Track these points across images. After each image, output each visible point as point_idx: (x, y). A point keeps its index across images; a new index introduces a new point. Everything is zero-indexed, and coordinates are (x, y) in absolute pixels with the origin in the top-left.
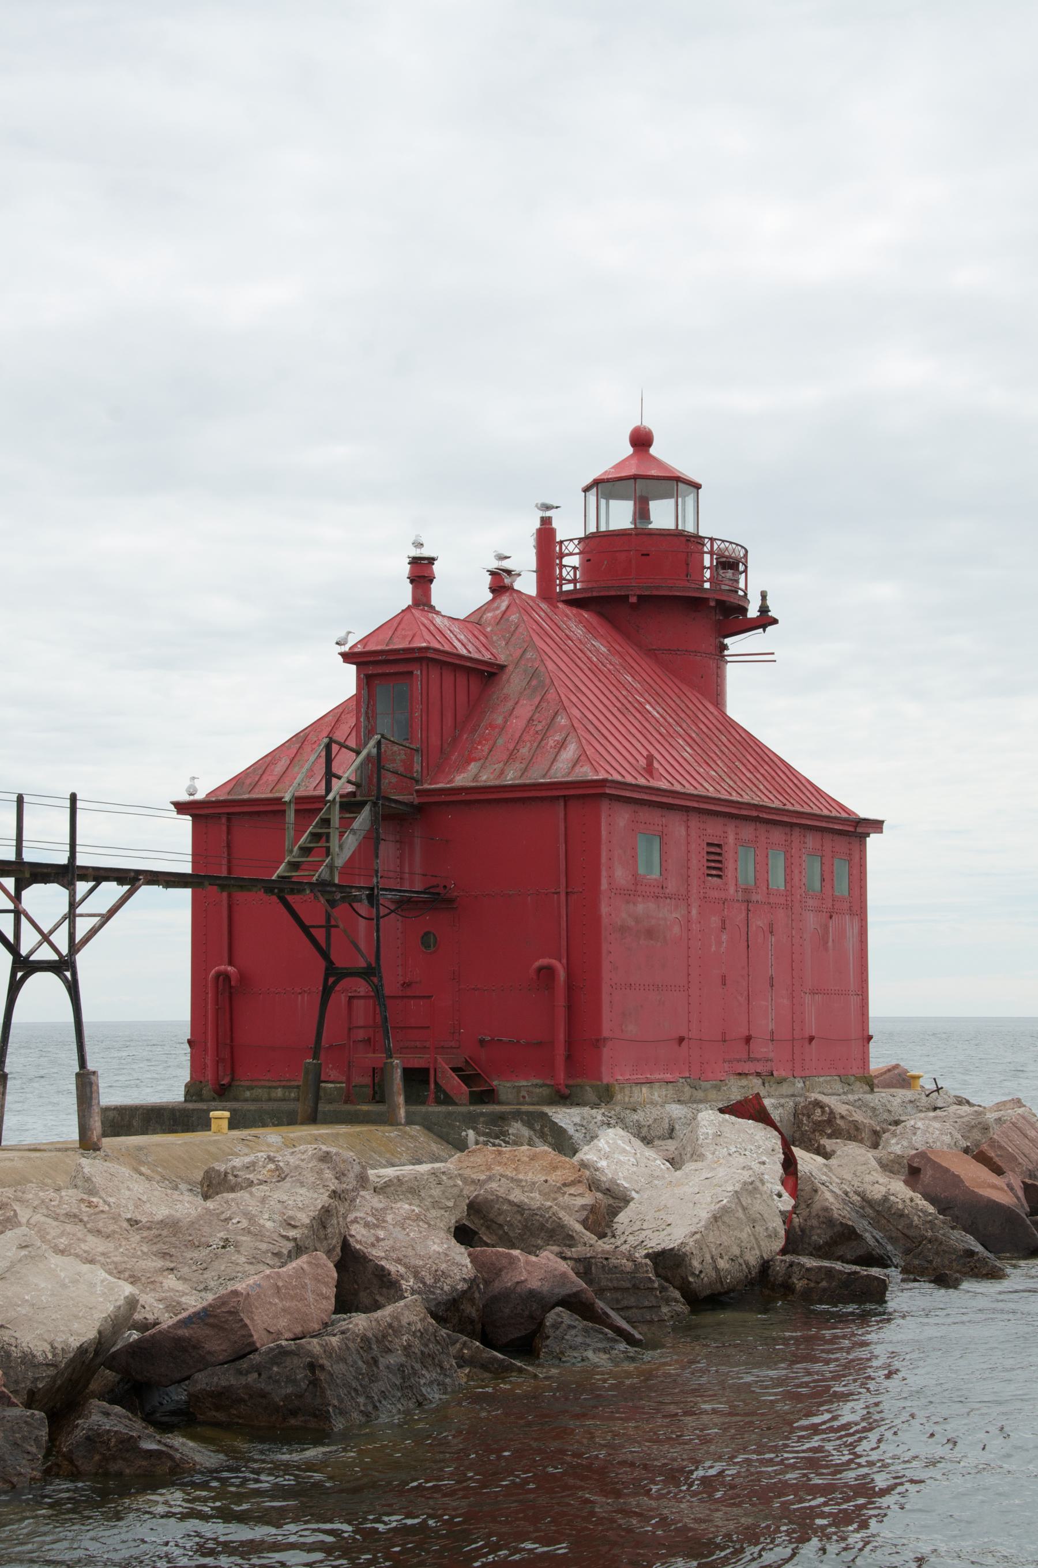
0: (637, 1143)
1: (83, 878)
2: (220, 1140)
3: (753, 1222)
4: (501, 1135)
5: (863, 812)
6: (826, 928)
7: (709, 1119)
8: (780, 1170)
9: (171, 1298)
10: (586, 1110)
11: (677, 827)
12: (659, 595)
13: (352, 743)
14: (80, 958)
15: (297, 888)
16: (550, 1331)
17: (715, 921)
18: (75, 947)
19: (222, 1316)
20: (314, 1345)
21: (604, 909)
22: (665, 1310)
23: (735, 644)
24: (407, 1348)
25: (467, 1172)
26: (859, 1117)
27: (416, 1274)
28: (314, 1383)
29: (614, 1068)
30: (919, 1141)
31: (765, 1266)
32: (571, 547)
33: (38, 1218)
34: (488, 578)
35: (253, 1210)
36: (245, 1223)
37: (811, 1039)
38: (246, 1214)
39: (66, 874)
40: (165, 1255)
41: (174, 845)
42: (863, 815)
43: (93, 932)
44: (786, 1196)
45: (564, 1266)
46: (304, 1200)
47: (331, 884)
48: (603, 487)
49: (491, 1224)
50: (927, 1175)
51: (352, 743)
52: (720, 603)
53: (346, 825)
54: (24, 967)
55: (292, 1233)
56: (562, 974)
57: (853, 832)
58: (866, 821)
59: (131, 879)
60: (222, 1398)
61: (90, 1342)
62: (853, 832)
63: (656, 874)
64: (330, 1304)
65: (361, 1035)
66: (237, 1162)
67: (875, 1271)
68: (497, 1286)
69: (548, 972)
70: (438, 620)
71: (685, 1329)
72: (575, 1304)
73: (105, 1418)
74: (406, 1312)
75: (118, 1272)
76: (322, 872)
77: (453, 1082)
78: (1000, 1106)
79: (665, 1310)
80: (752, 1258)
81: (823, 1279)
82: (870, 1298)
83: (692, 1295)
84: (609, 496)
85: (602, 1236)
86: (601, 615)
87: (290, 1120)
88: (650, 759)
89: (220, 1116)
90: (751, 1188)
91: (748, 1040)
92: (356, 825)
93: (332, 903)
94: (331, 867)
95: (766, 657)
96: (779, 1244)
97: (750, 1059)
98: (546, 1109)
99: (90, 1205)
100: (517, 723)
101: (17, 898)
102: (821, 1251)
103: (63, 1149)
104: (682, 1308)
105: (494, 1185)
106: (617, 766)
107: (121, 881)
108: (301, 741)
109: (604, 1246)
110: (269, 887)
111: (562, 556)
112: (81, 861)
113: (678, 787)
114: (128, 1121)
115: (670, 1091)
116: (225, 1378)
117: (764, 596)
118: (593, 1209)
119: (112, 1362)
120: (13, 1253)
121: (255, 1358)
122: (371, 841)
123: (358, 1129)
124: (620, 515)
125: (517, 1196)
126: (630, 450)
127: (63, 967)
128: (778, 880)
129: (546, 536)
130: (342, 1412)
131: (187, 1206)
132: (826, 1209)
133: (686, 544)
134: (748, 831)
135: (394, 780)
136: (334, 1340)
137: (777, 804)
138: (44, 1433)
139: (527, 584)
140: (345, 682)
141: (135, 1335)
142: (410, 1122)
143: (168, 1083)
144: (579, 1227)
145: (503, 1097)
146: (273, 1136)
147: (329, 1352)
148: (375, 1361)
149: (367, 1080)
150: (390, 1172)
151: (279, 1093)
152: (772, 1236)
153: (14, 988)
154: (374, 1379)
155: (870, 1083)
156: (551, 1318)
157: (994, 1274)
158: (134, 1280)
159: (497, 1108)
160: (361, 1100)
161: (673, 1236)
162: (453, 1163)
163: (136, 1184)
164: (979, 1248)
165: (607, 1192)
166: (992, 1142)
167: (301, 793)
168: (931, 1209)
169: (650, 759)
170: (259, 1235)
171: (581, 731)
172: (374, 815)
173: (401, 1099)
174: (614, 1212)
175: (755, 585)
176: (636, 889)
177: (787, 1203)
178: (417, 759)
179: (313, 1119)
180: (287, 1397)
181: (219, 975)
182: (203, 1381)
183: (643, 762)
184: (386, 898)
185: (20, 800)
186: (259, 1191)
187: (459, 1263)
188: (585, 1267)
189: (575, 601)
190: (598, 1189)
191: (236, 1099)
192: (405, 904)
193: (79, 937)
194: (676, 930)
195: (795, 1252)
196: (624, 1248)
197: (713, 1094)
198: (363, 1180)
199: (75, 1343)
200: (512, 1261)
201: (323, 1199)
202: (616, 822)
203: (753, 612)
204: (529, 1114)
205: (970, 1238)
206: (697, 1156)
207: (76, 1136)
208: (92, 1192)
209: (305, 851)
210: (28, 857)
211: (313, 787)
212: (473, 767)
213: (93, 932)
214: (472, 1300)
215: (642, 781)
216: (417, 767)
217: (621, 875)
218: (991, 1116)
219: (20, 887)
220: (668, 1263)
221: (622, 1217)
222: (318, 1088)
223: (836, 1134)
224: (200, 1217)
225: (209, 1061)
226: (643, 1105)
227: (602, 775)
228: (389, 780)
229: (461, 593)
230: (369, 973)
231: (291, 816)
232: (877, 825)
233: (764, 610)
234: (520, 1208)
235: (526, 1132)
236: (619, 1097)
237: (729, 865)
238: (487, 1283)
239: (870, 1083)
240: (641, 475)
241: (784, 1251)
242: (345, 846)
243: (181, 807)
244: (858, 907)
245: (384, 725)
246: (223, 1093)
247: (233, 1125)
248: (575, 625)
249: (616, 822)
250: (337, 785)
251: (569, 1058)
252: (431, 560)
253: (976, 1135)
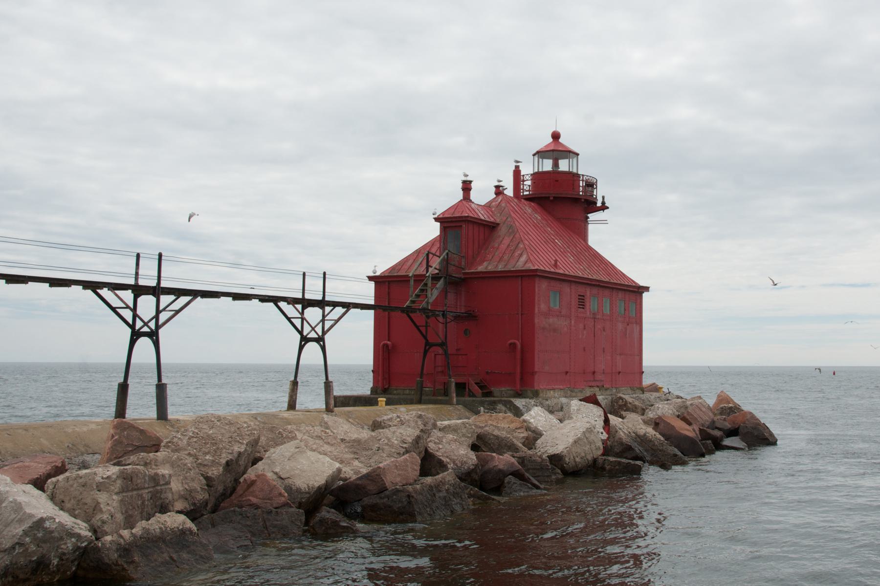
0: (547, 413)
2: (382, 410)
3: (590, 443)
4: (494, 409)
5: (642, 283)
6: (626, 329)
7: (575, 404)
8: (602, 423)
9: (355, 469)
10: (528, 400)
11: (566, 288)
12: (562, 196)
13: (438, 254)
14: (326, 337)
15: (414, 310)
16: (506, 485)
17: (581, 326)
19: (374, 476)
20: (410, 488)
21: (536, 321)
22: (554, 477)
23: (592, 216)
24: (447, 490)
25: (478, 423)
26: (637, 403)
27: (454, 462)
28: (410, 503)
29: (539, 383)
30: (659, 413)
31: (595, 460)
32: (527, 177)
33: (305, 437)
34: (494, 189)
35: (390, 436)
36: (386, 441)
37: (619, 373)
38: (387, 438)
39: (321, 304)
40: (355, 453)
41: (367, 293)
43: (332, 326)
44: (605, 433)
45: (513, 460)
46: (410, 433)
48: (541, 154)
49: (486, 443)
50: (661, 426)
51: (438, 254)
52: (586, 200)
53: (434, 285)
54: (305, 340)
55: (405, 445)
56: (519, 346)
57: (637, 291)
59: (347, 306)
60: (374, 507)
61: (323, 485)
62: (637, 291)
63: (557, 307)
64: (418, 473)
65: (440, 369)
66: (385, 418)
67: (639, 463)
68: (486, 467)
69: (513, 346)
70: (473, 205)
71: (559, 482)
72: (517, 474)
73: (327, 513)
74: (448, 476)
75: (335, 459)
76: (424, 305)
77: (475, 388)
78: (693, 399)
79: (554, 477)
80: (590, 457)
81: (618, 465)
82: (635, 472)
83: (564, 471)
84: (543, 158)
85: (530, 449)
86: (539, 204)
87: (411, 402)
88: (556, 261)
89: (382, 400)
90: (590, 430)
91: (594, 373)
92: (438, 286)
93: (428, 317)
94: (428, 303)
95: (604, 222)
96: (600, 452)
97: (594, 380)
98: (512, 400)
99: (326, 433)
100: (503, 246)
101: (302, 313)
102: (617, 455)
103: (319, 411)
104: (560, 476)
105: (487, 428)
106: (542, 263)
107: (343, 307)
108: (418, 252)
109: (530, 452)
110: (403, 310)
111: (524, 181)
112: (327, 299)
113: (567, 273)
115: (562, 393)
116: (375, 500)
117: (603, 197)
118: (527, 438)
119: (332, 493)
120: (293, 450)
121: (387, 493)
122: (444, 293)
123: (437, 406)
124: (547, 165)
125: (496, 432)
126: (551, 140)
127: (320, 340)
128: (607, 311)
129: (517, 172)
130: (420, 514)
131: (365, 434)
132: (620, 439)
133: (573, 177)
134: (595, 291)
135: (454, 268)
136: (418, 487)
137: (607, 280)
138: (303, 518)
139: (509, 192)
140: (434, 230)
141: (341, 483)
142: (457, 404)
143: (364, 388)
144: (520, 445)
145: (495, 394)
146: (402, 408)
147: (415, 491)
148: (434, 495)
149: (442, 387)
150: (446, 423)
151: (407, 392)
152: (598, 449)
153: (301, 348)
154: (433, 501)
155: (643, 390)
156: (507, 480)
157: (684, 463)
158: (341, 462)
159: (492, 399)
160: (438, 395)
161: (559, 448)
162: (473, 419)
163: (344, 426)
164: (679, 453)
165: (534, 432)
166: (688, 413)
167: (417, 273)
168: (662, 439)
169: (556, 261)
170: (392, 446)
171: (529, 250)
172: (445, 282)
173: (454, 395)
174: (536, 439)
175: (599, 193)
176: (549, 313)
177: (605, 436)
178: (463, 260)
179: (420, 402)
180: (398, 508)
181: (384, 345)
182: (366, 501)
183: (553, 262)
184: (450, 316)
186: (392, 429)
187: (472, 458)
188: (522, 461)
189: (528, 199)
190: (530, 430)
191: (390, 394)
192: (457, 318)
193: (326, 329)
194: (565, 329)
195: (608, 455)
196: (539, 454)
197: (579, 394)
198: (435, 426)
199: (317, 485)
200: (493, 457)
201: (417, 432)
202: (541, 286)
203: (599, 204)
204: (505, 401)
205: (676, 450)
206: (570, 418)
207: (324, 407)
208: (327, 428)
209: (418, 296)
210: (307, 296)
211: (421, 271)
212: (485, 264)
213: (332, 326)
214: (476, 473)
215: (552, 270)
216: (463, 263)
217: (543, 307)
218: (688, 403)
219: (303, 309)
220: (556, 459)
221: (539, 442)
222: (422, 390)
223: (628, 410)
224: (369, 439)
225: (380, 378)
226: (550, 398)
227: (536, 267)
228: (451, 269)
229: (482, 195)
230: (443, 345)
231: (412, 282)
232: (647, 289)
233: (603, 203)
234: (497, 437)
235: (504, 408)
236: (541, 395)
237: (587, 304)
238: (482, 466)
239: (643, 390)
240: (556, 150)
241: (603, 455)
242: (433, 294)
243: (371, 278)
244: (638, 320)
245: (451, 247)
246: (385, 391)
247: (387, 404)
248: (528, 208)
249: (541, 286)
250: (430, 269)
251: (522, 379)
252: (471, 182)
253: (683, 410)
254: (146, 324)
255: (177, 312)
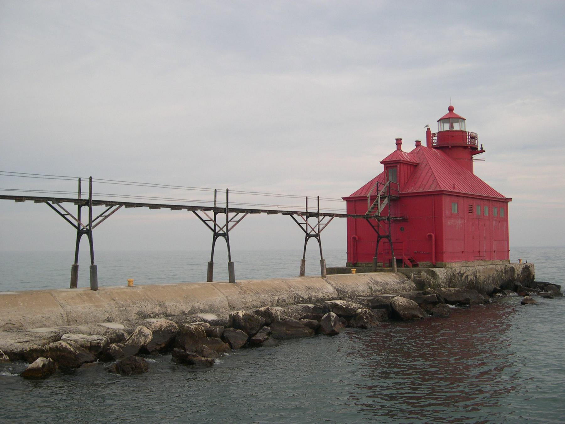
1: (321, 215)
11: (461, 201)
12: (455, 145)
14: (320, 234)
18: (319, 232)
21: (444, 221)
23: (475, 157)
39: (316, 215)
41: (342, 207)
42: (507, 197)
43: (324, 228)
47: (378, 216)
48: (442, 120)
51: (383, 183)
56: (433, 235)
57: (505, 201)
58: (508, 199)
59: (332, 215)
62: (505, 201)
63: (456, 212)
88: (454, 185)
91: (479, 252)
95: (482, 160)
107: (107, 205)
110: (364, 217)
113: (461, 191)
114: (332, 271)
117: (482, 145)
124: (446, 127)
127: (317, 236)
128: (487, 214)
129: (428, 132)
133: (463, 133)
139: (424, 144)
140: (381, 169)
142: (398, 271)
143: (343, 262)
153: (306, 241)
169: (454, 185)
172: (389, 200)
173: (396, 266)
175: (479, 143)
181: (353, 238)
185: (307, 198)
189: (436, 148)
202: (446, 200)
203: (479, 149)
213: (324, 228)
215: (452, 190)
229: (408, 148)
230: (388, 237)
231: (369, 200)
233: (482, 148)
240: (451, 116)
242: (381, 208)
243: (344, 199)
246: (355, 265)
254: (221, 229)
255: (238, 222)
